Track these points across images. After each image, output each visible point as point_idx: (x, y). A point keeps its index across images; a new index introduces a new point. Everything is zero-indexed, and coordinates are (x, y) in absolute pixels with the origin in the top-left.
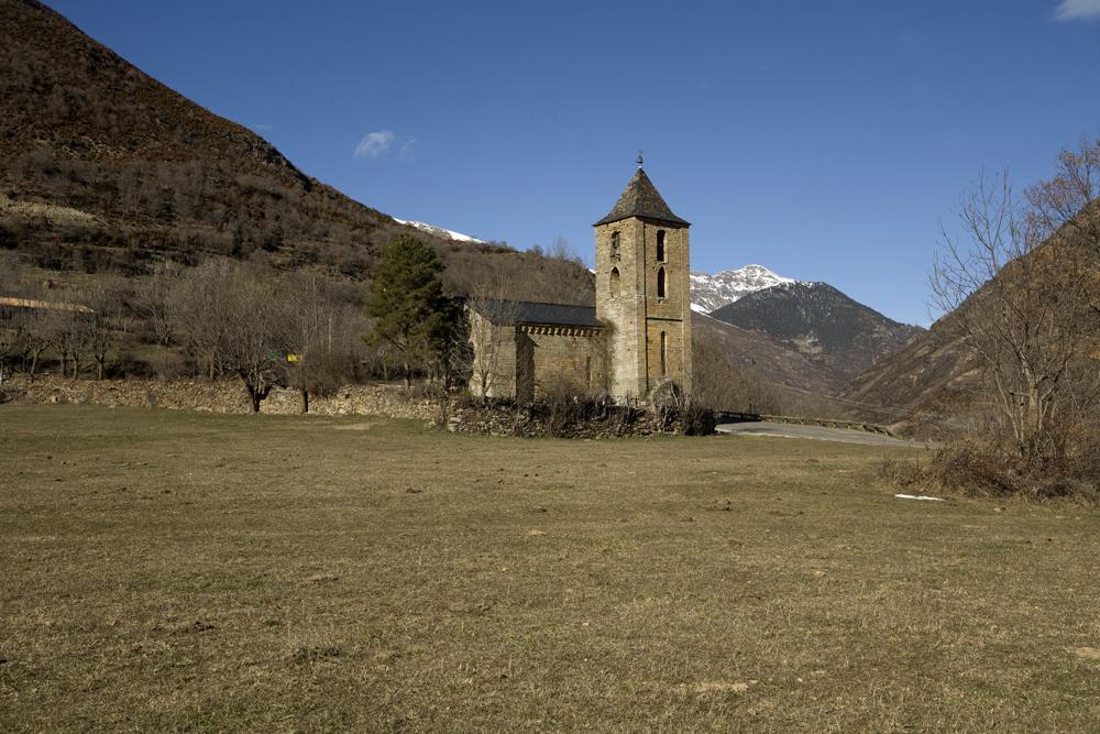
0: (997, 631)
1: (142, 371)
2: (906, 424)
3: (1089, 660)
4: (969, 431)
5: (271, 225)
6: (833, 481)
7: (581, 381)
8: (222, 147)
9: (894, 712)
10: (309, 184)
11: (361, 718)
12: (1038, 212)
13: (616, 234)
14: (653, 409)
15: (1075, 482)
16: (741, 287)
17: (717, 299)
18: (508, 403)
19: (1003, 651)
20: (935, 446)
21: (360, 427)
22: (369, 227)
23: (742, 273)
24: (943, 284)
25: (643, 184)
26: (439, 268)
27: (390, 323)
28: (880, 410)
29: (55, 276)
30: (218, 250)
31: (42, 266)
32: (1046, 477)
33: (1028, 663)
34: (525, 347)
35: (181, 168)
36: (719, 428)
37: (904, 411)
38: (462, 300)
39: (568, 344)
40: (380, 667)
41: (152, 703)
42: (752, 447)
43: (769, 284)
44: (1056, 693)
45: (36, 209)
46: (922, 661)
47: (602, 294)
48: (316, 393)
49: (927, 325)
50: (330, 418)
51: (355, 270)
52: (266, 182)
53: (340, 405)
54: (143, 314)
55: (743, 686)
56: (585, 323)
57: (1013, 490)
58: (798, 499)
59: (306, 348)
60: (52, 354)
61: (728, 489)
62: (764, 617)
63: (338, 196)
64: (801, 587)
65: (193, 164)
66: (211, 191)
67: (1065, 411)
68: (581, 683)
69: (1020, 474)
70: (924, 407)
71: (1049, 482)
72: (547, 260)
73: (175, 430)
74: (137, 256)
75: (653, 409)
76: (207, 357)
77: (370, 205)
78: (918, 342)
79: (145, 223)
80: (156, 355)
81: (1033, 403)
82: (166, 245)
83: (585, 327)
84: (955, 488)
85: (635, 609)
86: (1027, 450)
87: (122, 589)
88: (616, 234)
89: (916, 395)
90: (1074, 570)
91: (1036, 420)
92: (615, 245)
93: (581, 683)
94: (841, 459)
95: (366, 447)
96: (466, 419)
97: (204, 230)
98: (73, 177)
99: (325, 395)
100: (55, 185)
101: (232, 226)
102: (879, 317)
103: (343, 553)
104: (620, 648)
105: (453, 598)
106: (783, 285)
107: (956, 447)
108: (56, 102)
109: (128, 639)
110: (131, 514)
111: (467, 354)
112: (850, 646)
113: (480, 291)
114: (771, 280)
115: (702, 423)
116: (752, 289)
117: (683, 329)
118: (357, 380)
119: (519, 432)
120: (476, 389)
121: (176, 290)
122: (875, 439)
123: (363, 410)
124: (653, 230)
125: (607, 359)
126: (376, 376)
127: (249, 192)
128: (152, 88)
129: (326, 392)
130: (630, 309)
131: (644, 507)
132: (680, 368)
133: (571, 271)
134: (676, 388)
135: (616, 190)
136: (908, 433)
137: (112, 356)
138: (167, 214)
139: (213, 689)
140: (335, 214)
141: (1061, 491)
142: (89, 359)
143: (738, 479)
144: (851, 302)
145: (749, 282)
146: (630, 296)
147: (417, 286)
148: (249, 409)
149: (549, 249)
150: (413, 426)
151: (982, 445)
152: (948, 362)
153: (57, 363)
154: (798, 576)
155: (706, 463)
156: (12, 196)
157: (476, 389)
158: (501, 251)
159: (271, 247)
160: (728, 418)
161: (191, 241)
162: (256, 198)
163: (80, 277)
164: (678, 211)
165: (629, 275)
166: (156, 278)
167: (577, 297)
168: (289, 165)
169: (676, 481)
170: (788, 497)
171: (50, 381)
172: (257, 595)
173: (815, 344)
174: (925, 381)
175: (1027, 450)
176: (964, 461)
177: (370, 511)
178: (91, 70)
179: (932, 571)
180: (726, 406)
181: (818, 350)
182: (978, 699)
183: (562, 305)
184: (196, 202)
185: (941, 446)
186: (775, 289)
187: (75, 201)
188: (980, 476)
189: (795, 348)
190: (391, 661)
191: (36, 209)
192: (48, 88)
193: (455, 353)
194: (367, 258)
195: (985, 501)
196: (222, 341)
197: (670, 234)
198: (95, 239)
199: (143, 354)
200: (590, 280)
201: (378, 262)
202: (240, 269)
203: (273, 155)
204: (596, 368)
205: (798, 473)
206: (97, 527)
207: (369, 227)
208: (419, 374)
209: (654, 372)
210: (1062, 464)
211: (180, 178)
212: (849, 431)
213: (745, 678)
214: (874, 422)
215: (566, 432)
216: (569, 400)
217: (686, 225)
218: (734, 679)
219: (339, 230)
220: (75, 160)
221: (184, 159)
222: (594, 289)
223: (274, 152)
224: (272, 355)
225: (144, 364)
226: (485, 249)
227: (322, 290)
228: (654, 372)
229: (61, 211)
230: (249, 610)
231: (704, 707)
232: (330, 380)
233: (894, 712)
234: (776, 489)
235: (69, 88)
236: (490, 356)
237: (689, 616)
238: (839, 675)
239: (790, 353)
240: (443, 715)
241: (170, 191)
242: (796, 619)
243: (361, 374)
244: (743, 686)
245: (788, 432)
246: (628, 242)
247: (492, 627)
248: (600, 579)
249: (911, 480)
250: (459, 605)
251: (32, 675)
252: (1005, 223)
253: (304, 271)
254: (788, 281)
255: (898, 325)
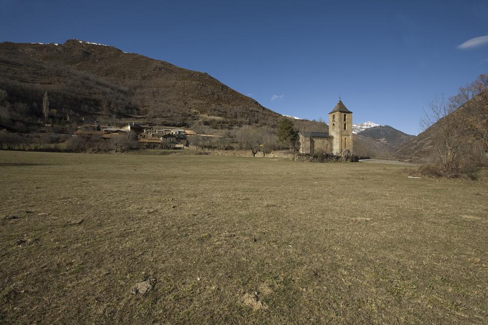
0: (438, 210)
1: (232, 148)
2: (410, 160)
3: (466, 218)
4: (428, 161)
5: (256, 117)
6: (391, 173)
7: (325, 150)
8: (246, 102)
9: (410, 227)
10: (264, 109)
11: (281, 219)
12: (452, 104)
13: (334, 116)
14: (343, 156)
15: (461, 174)
16: (365, 127)
17: (359, 130)
18: (308, 155)
19: (440, 215)
20: (419, 165)
21: (276, 160)
22: (277, 117)
23: (366, 124)
24: (423, 124)
25: (341, 104)
26: (292, 125)
27: (282, 138)
28: (402, 156)
29: (216, 130)
30: (246, 123)
31: (213, 128)
32: (452, 173)
33: (448, 218)
34: (312, 142)
35: (239, 107)
36: (359, 161)
37: (409, 157)
38: (298, 132)
39: (322, 141)
40: (284, 209)
41: (240, 212)
42: (368, 165)
43: (372, 126)
44: (456, 226)
45: (213, 117)
46: (417, 216)
47: (330, 130)
48: (266, 153)
49: (417, 135)
50: (269, 158)
51: (274, 126)
52: (255, 109)
53: (271, 155)
54: (232, 137)
55: (369, 219)
56: (326, 136)
57: (442, 176)
58: (381, 177)
59: (264, 143)
60: (216, 145)
61: (363, 174)
62: (374, 204)
63: (270, 111)
64: (383, 197)
65: (241, 106)
66: (244, 111)
67: (458, 156)
68: (329, 216)
69: (444, 172)
70: (415, 155)
71: (453, 174)
72: (317, 122)
73: (238, 160)
74: (231, 126)
75: (343, 156)
76: (244, 146)
77: (277, 112)
78: (414, 139)
79: (232, 119)
80: (234, 145)
81: (449, 154)
82: (236, 123)
83: (326, 137)
84: (425, 175)
85: (340, 201)
86: (447, 166)
87: (232, 191)
88: (334, 116)
89: (413, 153)
90: (461, 196)
91: (450, 158)
92: (334, 118)
93: (329, 216)
94: (392, 168)
95: (277, 164)
96: (299, 158)
97: (243, 120)
98: (219, 111)
99: (268, 153)
100: (216, 113)
101: (248, 118)
102: (403, 133)
103: (274, 186)
104: (338, 209)
105: (298, 196)
106: (376, 126)
107: (425, 165)
108: (216, 96)
109: (234, 200)
110: (232, 176)
111: (299, 144)
112: (397, 212)
113: (302, 130)
114: (373, 125)
115: (355, 159)
116: (368, 127)
117: (351, 137)
118: (275, 150)
119: (311, 161)
120: (301, 152)
121: (238, 132)
122: (401, 163)
123: (276, 156)
124: (343, 114)
125: (332, 145)
126: (279, 149)
127: (252, 111)
128: (233, 91)
129: (268, 153)
130: (337, 133)
131: (342, 178)
132: (350, 146)
133: (323, 125)
134: (349, 151)
135: (334, 105)
136: (411, 162)
137: (226, 146)
138: (236, 117)
139: (251, 211)
140: (270, 115)
141: (457, 176)
142: (222, 146)
143: (366, 172)
144: (395, 130)
145: (367, 126)
146: (337, 130)
147: (287, 129)
148: (253, 156)
149: (317, 120)
150: (287, 160)
151: (433, 165)
152: (423, 144)
153: (216, 147)
154: (382, 195)
155: (357, 168)
156: (208, 115)
157: (301, 152)
158: (306, 121)
159: (256, 122)
160: (362, 158)
161: (240, 122)
162: (253, 112)
163: (220, 130)
164: (349, 110)
165: (337, 125)
166: (234, 130)
167: (324, 130)
168: (260, 105)
169: (349, 172)
170: (378, 177)
171: (216, 151)
172: (257, 193)
173: (385, 140)
174: (416, 149)
175: (447, 166)
176: (428, 168)
177: (279, 177)
178: (222, 89)
179: (419, 195)
180: (361, 155)
181: (386, 141)
182: (433, 226)
183: (321, 132)
184: (241, 114)
185: (421, 165)
186: (374, 127)
187: (219, 115)
188: (435, 173)
189: (379, 141)
190: (286, 208)
191: (213, 117)
192: (214, 94)
193: (296, 144)
194: (276, 124)
195: (434, 179)
196: (247, 142)
197: (347, 115)
198: (223, 123)
199: (232, 145)
200: (328, 127)
201: (279, 124)
202: (250, 127)
203: (257, 103)
204: (329, 146)
205: (381, 171)
206: (226, 179)
207: (277, 117)
208: (288, 149)
209: (343, 147)
210: (457, 170)
211: (238, 109)
212: (394, 161)
213: (370, 217)
214: (401, 159)
215: (322, 161)
216: (323, 154)
217: (352, 113)
218: (367, 217)
219: (270, 118)
220: (219, 107)
221: (239, 105)
222: (328, 129)
223: (257, 102)
224: (257, 145)
225: (232, 147)
226: (303, 121)
227: (267, 131)
228: (343, 147)
229: (217, 117)
230: (256, 196)
231: (360, 223)
232: (269, 150)
233: (410, 227)
234: (375, 175)
235: (219, 94)
236: (304, 144)
237: (355, 203)
238: (394, 218)
239: (378, 143)
240: (298, 219)
241: (236, 112)
242: (382, 205)
243: (276, 149)
244: (369, 219)
245: (378, 162)
246: (337, 117)
247: (308, 202)
248: (332, 193)
249: (413, 173)
250: (300, 198)
251: (218, 205)
252: (442, 107)
253: (263, 127)
254: (377, 125)
255: (408, 135)
